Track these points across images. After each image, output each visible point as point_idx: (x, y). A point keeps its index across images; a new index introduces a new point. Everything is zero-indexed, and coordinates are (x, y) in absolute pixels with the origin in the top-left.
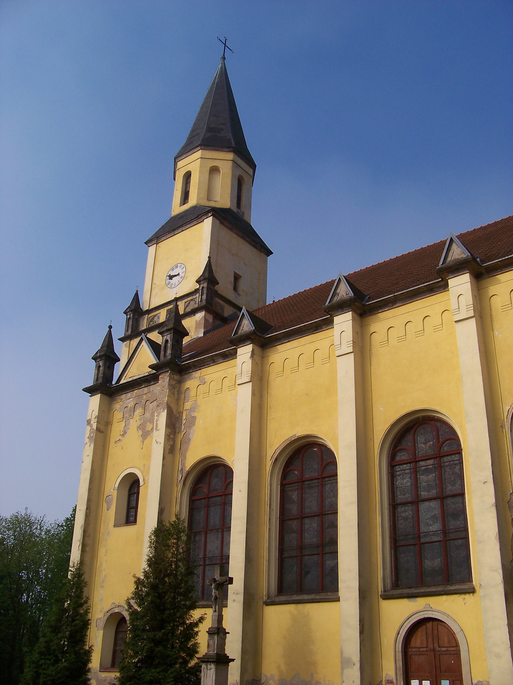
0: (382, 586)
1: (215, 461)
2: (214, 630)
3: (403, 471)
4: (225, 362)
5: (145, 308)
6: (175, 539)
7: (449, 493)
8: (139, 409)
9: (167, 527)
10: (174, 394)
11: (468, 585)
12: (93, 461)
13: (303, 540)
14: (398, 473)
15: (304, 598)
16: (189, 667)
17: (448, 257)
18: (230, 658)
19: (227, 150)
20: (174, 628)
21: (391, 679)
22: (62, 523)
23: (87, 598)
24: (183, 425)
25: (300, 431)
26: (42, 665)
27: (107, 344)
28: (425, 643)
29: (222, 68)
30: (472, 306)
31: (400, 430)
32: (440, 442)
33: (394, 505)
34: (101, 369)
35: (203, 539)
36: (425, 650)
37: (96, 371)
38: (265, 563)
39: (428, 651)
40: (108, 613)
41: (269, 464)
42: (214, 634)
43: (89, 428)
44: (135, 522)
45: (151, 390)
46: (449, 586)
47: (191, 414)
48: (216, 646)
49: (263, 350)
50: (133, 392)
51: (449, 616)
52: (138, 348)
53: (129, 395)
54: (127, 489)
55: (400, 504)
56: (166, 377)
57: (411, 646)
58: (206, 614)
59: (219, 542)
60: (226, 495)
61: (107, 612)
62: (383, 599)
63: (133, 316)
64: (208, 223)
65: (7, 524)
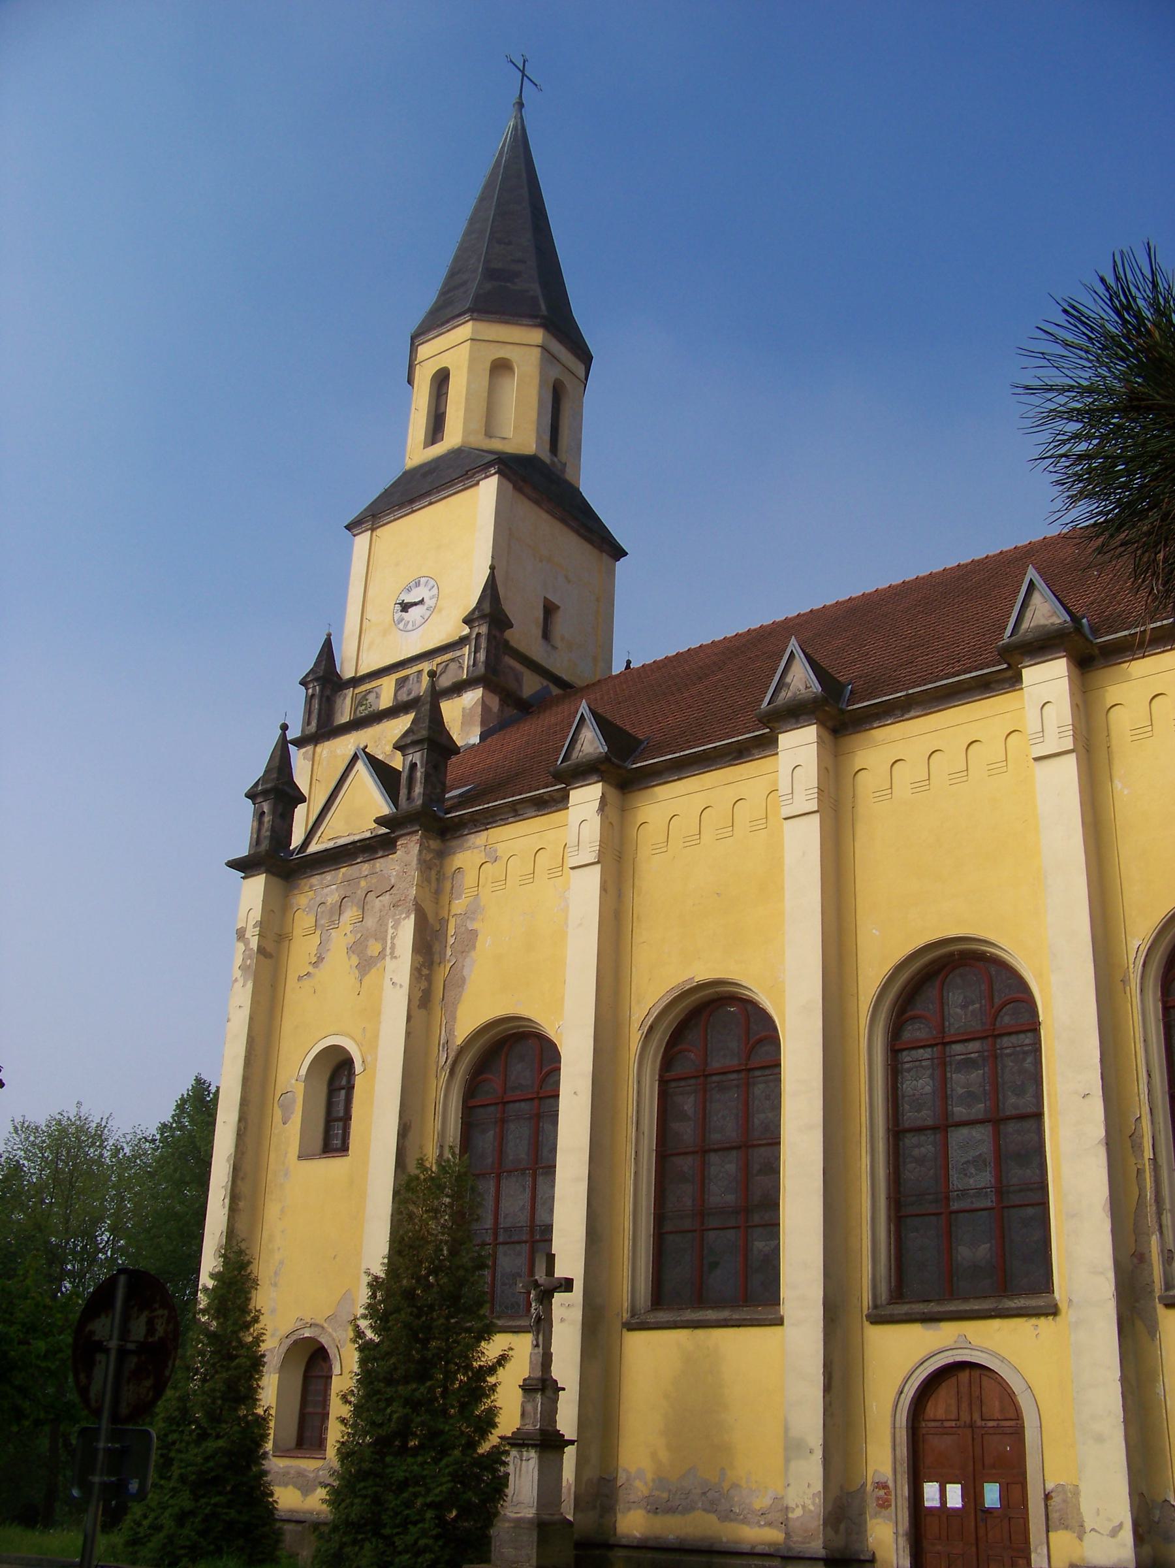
0: (870, 1297)
2: (534, 1382)
3: (917, 1063)
4: (541, 815)
5: (348, 673)
6: (448, 1196)
7: (1010, 1112)
9: (432, 1172)
10: (429, 881)
12: (251, 1018)
13: (706, 1197)
14: (907, 1066)
16: (478, 1453)
17: (1023, 620)
18: (566, 1438)
19: (531, 323)
20: (450, 1377)
21: (883, 1480)
22: (153, 1135)
23: (257, 1311)
24: (448, 948)
25: (703, 972)
26: (174, 1443)
28: (954, 1409)
29: (515, 128)
30: (1071, 727)
31: (912, 979)
32: (996, 1006)
33: (897, 1132)
34: (267, 819)
35: (492, 1190)
36: (954, 1425)
37: (256, 824)
39: (959, 1427)
40: (288, 1340)
41: (635, 1038)
42: (535, 1390)
43: (241, 947)
44: (344, 1149)
46: (1005, 1300)
47: (468, 925)
48: (539, 1416)
49: (624, 794)
50: (337, 871)
51: (1005, 1361)
52: (348, 776)
53: (328, 877)
54: (326, 1076)
55: (910, 1130)
56: (412, 844)
57: (926, 1418)
58: (512, 1349)
59: (527, 1194)
61: (287, 1337)
62: (872, 1323)
63: (322, 691)
64: (488, 489)
65: (40, 1139)
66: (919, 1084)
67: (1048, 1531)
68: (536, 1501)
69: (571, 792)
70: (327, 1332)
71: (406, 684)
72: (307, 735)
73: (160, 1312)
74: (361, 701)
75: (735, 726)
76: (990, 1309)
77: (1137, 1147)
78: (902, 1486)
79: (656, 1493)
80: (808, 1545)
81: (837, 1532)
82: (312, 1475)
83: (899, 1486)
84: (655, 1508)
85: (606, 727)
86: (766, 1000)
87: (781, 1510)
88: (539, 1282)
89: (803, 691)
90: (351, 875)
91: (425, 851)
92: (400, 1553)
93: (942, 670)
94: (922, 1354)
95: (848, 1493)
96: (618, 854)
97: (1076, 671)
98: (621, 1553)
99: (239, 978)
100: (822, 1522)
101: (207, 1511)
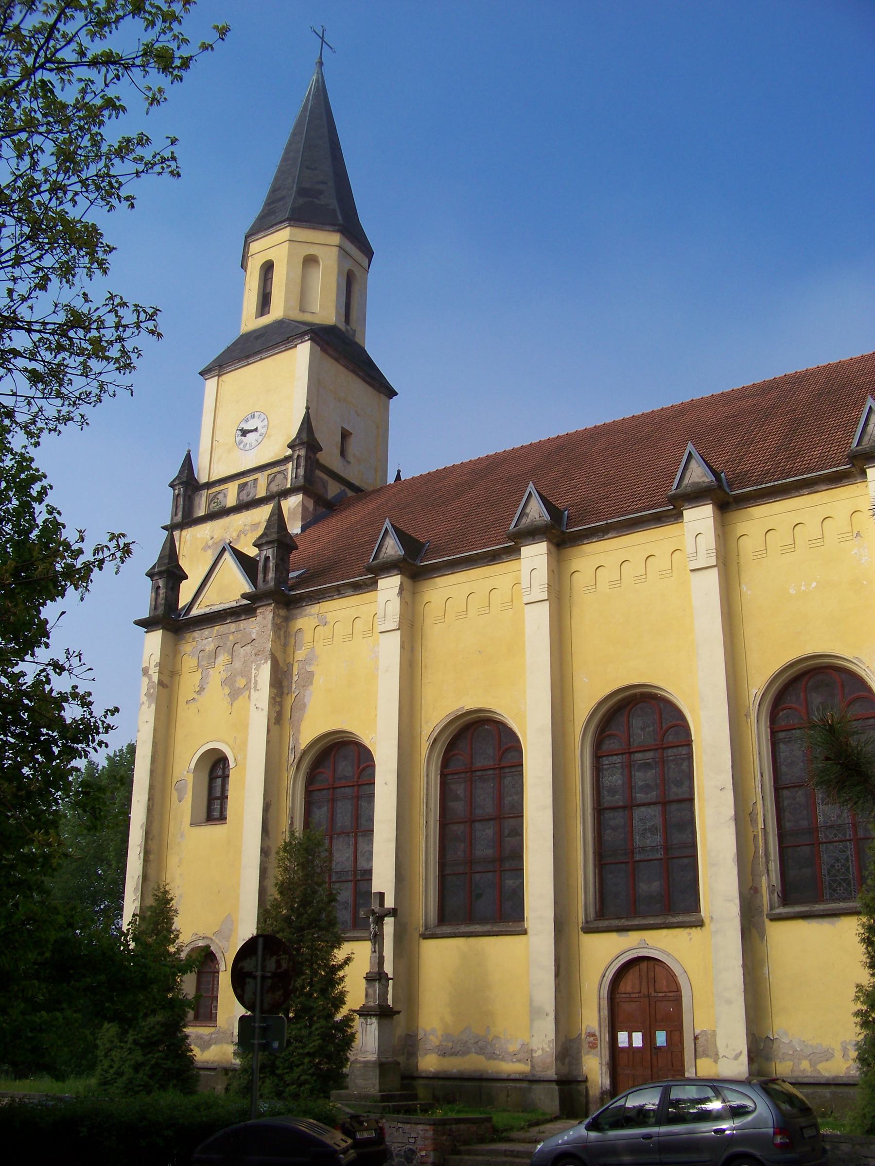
0: (583, 916)
1: (343, 737)
2: (373, 975)
3: (612, 765)
5: (203, 479)
7: (672, 797)
8: (224, 655)
10: (279, 637)
11: (695, 917)
13: (473, 851)
15: (477, 930)
19: (331, 229)
25: (471, 702)
27: (168, 553)
29: (317, 81)
30: (715, 551)
33: (600, 810)
34: (162, 591)
36: (637, 996)
37: (154, 595)
38: (422, 883)
40: (187, 948)
42: (374, 980)
43: (146, 680)
44: (222, 818)
45: (242, 628)
49: (415, 582)
50: (212, 628)
52: (218, 562)
53: (206, 632)
56: (268, 612)
57: (620, 992)
59: (352, 848)
60: (359, 785)
62: (585, 933)
63: (185, 491)
64: (303, 351)
66: (614, 778)
67: (696, 1059)
68: (377, 1049)
69: (379, 581)
70: (214, 942)
71: (246, 488)
72: (175, 523)
73: (284, 956)
74: (212, 499)
75: (489, 538)
76: (660, 923)
77: (754, 821)
78: (605, 1035)
79: (444, 1043)
80: (545, 1073)
81: (563, 1064)
82: (207, 1038)
83: (603, 1036)
84: (444, 1053)
85: (403, 537)
86: (512, 723)
87: (527, 1052)
88: (375, 911)
89: (538, 518)
90: (222, 632)
91: (276, 618)
92: (288, 1085)
93: (629, 506)
94: (617, 952)
95: (570, 1040)
96: (410, 623)
97: (717, 512)
98: (421, 1082)
99: (145, 702)
100: (554, 1058)
101: (153, 1062)
